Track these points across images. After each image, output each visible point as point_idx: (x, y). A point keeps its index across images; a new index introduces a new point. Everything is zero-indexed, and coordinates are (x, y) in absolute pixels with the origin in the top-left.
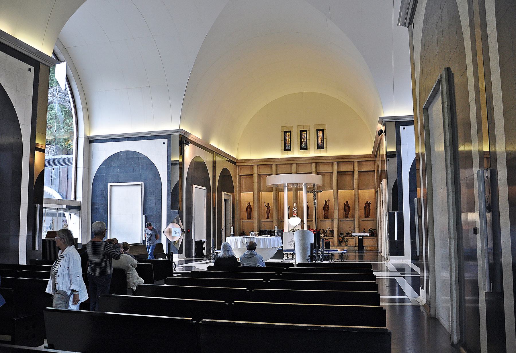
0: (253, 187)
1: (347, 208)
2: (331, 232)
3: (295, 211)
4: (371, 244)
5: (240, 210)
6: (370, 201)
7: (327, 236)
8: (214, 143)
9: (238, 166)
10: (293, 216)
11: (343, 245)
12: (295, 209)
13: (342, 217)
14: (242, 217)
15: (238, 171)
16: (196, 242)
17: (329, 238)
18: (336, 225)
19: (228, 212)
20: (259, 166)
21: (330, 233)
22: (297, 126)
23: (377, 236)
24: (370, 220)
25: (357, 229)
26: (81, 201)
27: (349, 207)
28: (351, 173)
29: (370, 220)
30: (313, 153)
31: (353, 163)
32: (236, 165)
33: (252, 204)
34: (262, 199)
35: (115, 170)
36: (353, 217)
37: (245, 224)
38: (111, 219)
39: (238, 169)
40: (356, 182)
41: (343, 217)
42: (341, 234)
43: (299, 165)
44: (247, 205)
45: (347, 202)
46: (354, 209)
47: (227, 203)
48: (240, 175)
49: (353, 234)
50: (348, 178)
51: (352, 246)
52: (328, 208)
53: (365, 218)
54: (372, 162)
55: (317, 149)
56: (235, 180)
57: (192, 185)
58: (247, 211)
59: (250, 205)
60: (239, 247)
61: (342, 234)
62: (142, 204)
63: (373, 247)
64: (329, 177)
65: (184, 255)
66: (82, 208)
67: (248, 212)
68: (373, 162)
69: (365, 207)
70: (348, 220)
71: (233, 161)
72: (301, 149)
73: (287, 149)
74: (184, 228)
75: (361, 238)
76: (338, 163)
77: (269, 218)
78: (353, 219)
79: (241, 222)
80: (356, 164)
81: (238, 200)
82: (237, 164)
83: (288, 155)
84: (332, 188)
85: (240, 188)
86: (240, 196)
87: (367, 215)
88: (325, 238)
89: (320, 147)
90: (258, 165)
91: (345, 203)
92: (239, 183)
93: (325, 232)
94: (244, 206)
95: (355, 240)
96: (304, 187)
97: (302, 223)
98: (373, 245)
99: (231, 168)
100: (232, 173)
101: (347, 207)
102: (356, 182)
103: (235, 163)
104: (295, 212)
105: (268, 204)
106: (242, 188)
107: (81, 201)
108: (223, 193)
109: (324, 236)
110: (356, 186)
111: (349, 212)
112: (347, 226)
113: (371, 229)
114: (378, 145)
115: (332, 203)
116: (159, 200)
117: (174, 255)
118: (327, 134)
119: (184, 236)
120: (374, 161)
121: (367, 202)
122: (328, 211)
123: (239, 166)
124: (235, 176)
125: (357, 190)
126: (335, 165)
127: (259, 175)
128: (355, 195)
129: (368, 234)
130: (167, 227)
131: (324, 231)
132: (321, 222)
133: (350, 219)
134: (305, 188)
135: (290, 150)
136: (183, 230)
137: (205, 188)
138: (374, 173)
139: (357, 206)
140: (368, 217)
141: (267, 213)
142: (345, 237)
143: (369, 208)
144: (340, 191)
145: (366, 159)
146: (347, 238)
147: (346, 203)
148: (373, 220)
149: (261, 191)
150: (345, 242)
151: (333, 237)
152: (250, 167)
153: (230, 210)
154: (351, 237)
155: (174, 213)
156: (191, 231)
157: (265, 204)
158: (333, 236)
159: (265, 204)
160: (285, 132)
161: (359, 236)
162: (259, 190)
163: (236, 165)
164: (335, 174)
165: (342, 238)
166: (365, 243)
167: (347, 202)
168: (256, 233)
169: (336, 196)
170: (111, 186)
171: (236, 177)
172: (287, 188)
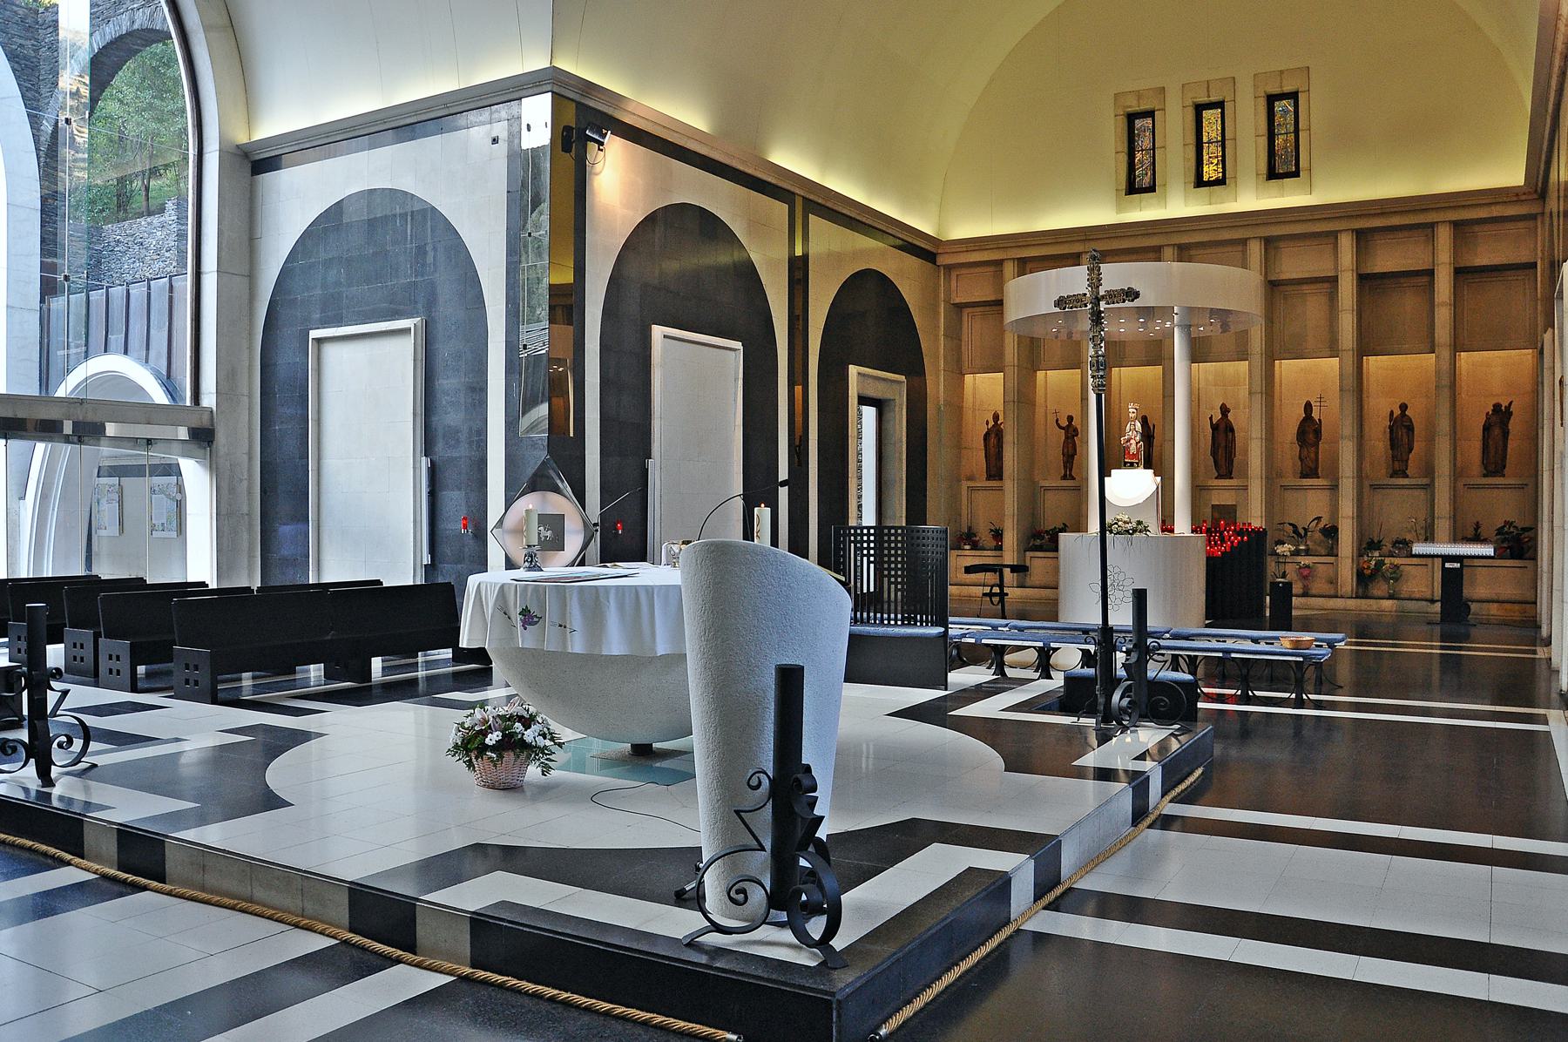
0: (1000, 354)
1: (1401, 433)
2: (1324, 535)
3: (1132, 441)
4: (1509, 591)
5: (959, 445)
6: (1511, 403)
7: (1307, 553)
8: (790, 158)
9: (944, 266)
10: (1125, 463)
11: (1376, 592)
12: (1132, 435)
13: (1380, 474)
17: (1316, 559)
18: (1347, 507)
19: (889, 450)
21: (1322, 538)
22: (1183, 86)
23: (1534, 558)
24: (1507, 487)
25: (1443, 526)
26: (215, 409)
27: (1410, 429)
28: (1425, 279)
29: (1507, 487)
30: (1251, 198)
31: (1430, 235)
35: (332, 275)
36: (1429, 471)
37: (980, 497)
38: (321, 478)
40: (1443, 316)
41: (1384, 471)
42: (1367, 544)
45: (1404, 407)
46: (1431, 439)
47: (887, 416)
48: (960, 307)
49: (1418, 549)
50: (1406, 304)
51: (1418, 596)
52: (1318, 433)
53: (1485, 476)
54: (1521, 224)
58: (985, 446)
61: (1374, 545)
62: (418, 411)
63: (1517, 607)
64: (1323, 299)
66: (221, 437)
67: (993, 451)
68: (1531, 224)
69: (1487, 428)
70: (1403, 487)
71: (922, 249)
73: (1136, 186)
75: (1457, 565)
76: (1362, 236)
77: (1070, 475)
78: (1425, 481)
80: (1444, 236)
82: (941, 260)
83: (1145, 211)
84: (1333, 351)
87: (1494, 463)
88: (1299, 559)
89: (1278, 170)
91: (1392, 413)
93: (1299, 534)
94: (977, 429)
95: (1430, 574)
97: (1165, 494)
98: (1518, 598)
99: (905, 275)
100: (910, 292)
101: (1401, 427)
102: (1443, 316)
107: (215, 409)
109: (1296, 553)
110: (1443, 333)
111: (1411, 450)
112: (1397, 511)
113: (1510, 524)
114: (1550, 110)
115: (1335, 415)
116: (478, 391)
118: (1317, 112)
120: (1533, 217)
121: (1497, 407)
122: (1316, 445)
123: (949, 268)
125: (1446, 353)
126: (1346, 243)
128: (1438, 372)
129: (1488, 550)
131: (1296, 531)
132: (1288, 494)
133: (1413, 481)
134: (1180, 336)
138: (1532, 278)
139: (1444, 425)
141: (1063, 454)
142: (1387, 561)
143: (1505, 434)
144: (1373, 363)
145: (1496, 211)
146: (1397, 561)
147: (1397, 412)
148: (1522, 487)
150: (1386, 580)
151: (1331, 559)
154: (1408, 561)
157: (1057, 421)
158: (1332, 552)
159: (1057, 421)
161: (1447, 558)
165: (1373, 563)
166: (1478, 588)
167: (1404, 407)
168: (677, 551)
169: (1350, 382)
170: (319, 341)
171: (939, 313)
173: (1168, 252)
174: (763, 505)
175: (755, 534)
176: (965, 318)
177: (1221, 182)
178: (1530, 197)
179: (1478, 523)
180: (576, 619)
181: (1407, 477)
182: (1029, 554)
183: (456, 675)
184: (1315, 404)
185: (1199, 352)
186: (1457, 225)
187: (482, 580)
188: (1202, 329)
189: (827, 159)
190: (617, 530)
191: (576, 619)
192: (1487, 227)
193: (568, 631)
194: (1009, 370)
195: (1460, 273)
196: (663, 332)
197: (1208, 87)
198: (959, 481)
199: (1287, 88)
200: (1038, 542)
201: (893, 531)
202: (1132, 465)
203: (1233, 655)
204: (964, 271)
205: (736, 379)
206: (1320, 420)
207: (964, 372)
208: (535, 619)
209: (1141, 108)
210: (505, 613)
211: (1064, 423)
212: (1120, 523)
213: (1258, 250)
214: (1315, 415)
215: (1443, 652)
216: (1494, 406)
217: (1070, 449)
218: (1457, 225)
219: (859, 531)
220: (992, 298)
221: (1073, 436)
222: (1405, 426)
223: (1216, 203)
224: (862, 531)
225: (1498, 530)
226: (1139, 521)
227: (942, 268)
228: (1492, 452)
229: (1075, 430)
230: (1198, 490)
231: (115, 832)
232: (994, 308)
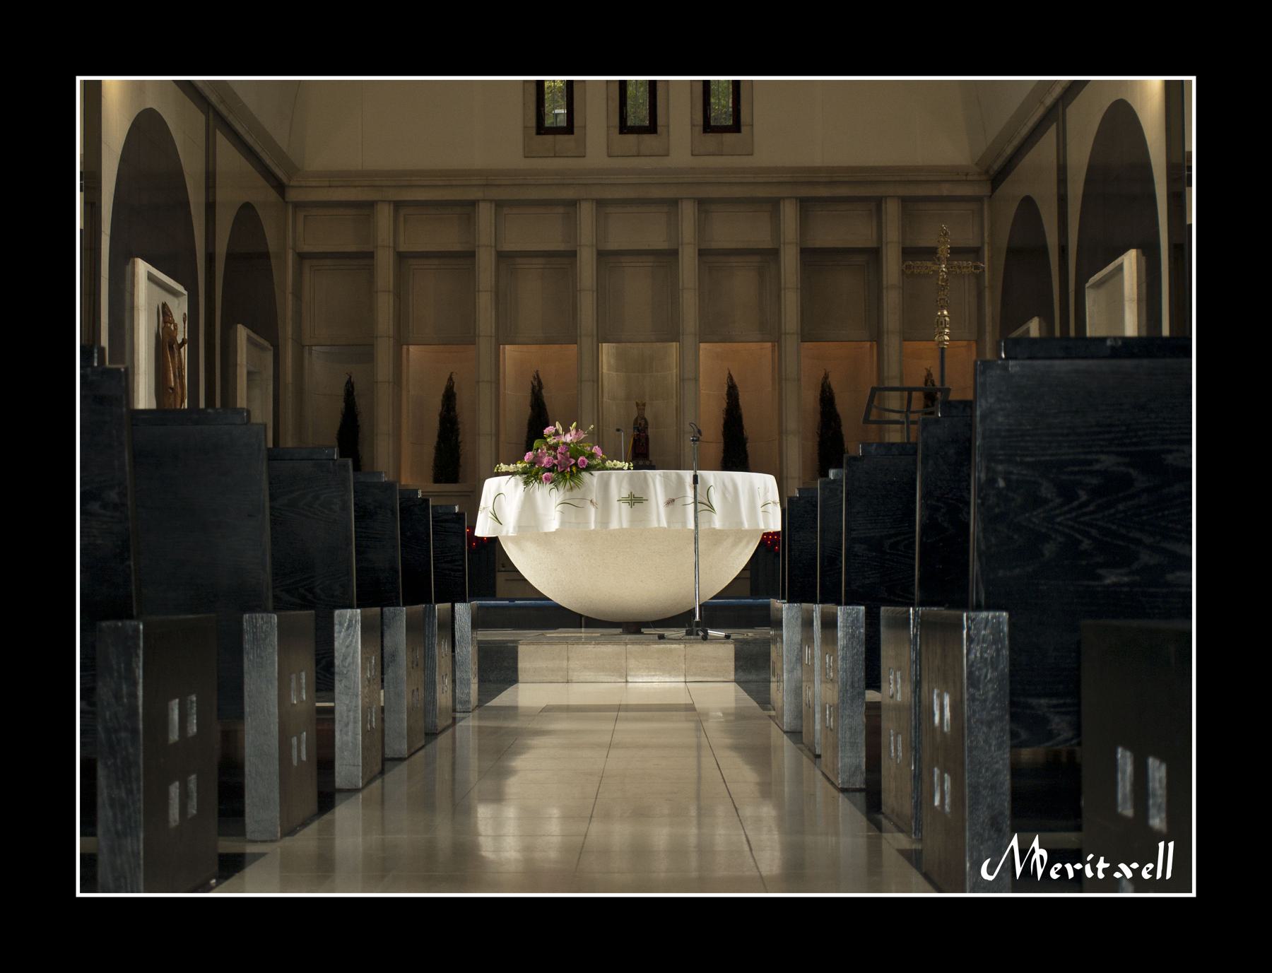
40: (892, 300)
48: (302, 257)
56: (285, 274)
82: (293, 195)
108: (242, 333)
123: (298, 206)
127: (402, 258)
137: (180, 288)
145: (946, 190)
160: (569, 129)
164: (790, 260)
218: (905, 201)
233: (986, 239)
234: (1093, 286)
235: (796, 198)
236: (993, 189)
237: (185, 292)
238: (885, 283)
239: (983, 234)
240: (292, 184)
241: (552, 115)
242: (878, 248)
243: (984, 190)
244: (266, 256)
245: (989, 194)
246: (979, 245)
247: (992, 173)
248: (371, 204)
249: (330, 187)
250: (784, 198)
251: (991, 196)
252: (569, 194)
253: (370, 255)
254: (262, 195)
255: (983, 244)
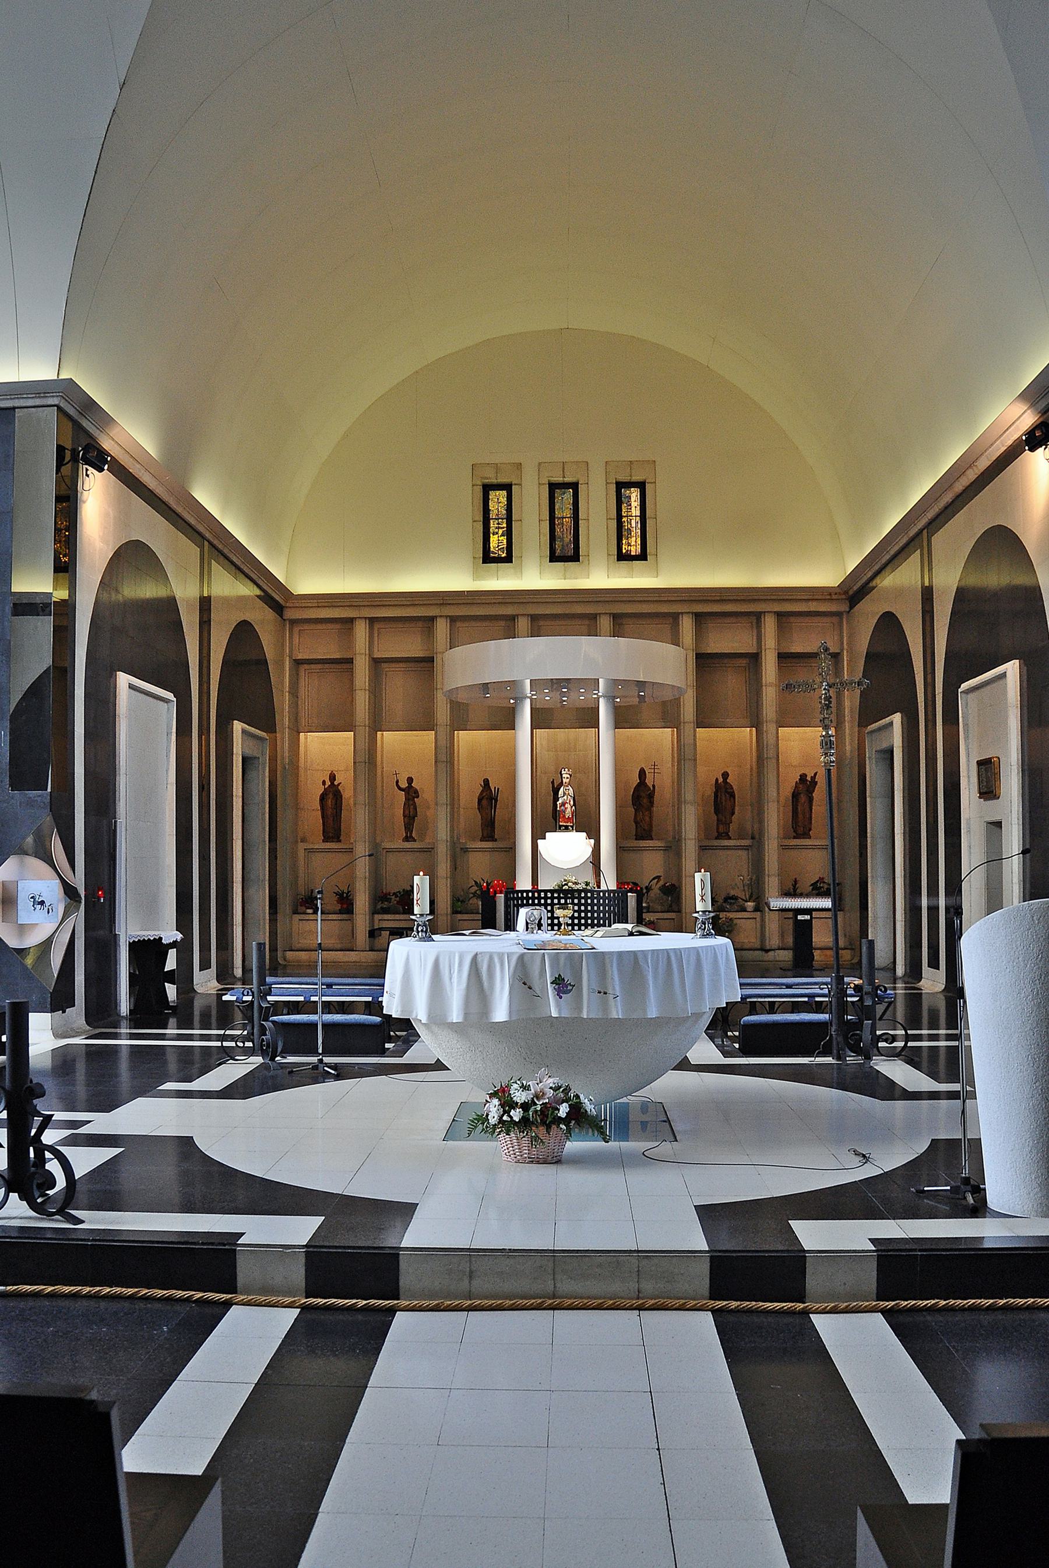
0: (351, 713)
5: (297, 807)
6: (816, 774)
8: (206, 496)
10: (560, 826)
14: (300, 835)
15: (291, 642)
16: (137, 947)
18: (362, 868)
20: (376, 626)
29: (814, 847)
32: (281, 616)
33: (345, 780)
34: (382, 761)
37: (317, 859)
39: (291, 637)
40: (770, 695)
43: (541, 623)
44: (324, 783)
45: (725, 775)
47: (252, 774)
48: (298, 663)
52: (651, 796)
54: (828, 619)
55: (618, 560)
56: (281, 679)
57: (112, 676)
59: (336, 783)
60: (500, 1013)
65: (77, 1014)
68: (835, 619)
69: (795, 795)
70: (728, 848)
72: (554, 558)
74: (79, 882)
75: (808, 917)
76: (699, 618)
77: (411, 836)
79: (301, 854)
80: (770, 625)
81: (291, 762)
82: (289, 614)
85: (297, 713)
86: (295, 744)
90: (372, 621)
91: (717, 780)
92: (294, 692)
94: (313, 789)
96: (601, 700)
103: (278, 608)
104: (569, 810)
105: (410, 780)
106: (302, 714)
108: (238, 726)
111: (733, 813)
117: (32, 1017)
118: (661, 497)
119: (79, 918)
121: (803, 777)
123: (293, 622)
124: (280, 664)
127: (376, 663)
130: (449, 1069)
135: (508, 559)
136: (70, 891)
137: (170, 696)
140: (806, 835)
141: (404, 816)
143: (811, 800)
145: (813, 607)
146: (732, 915)
147: (721, 780)
148: (746, 848)
149: (383, 728)
152: (338, 626)
153: (264, 802)
155: (31, 803)
156: (108, 897)
157: (397, 782)
159: (397, 782)
160: (487, 489)
162: (377, 724)
163: (281, 616)
168: (558, 912)
172: (528, 702)
173: (523, 624)
174: (421, 873)
175: (415, 902)
176: (302, 673)
177: (643, 556)
178: (840, 597)
179: (796, 879)
180: (616, 985)
181: (730, 838)
182: (377, 917)
183: (947, 1035)
184: (650, 771)
185: (623, 719)
186: (779, 615)
187: (479, 950)
188: (618, 700)
189: (226, 503)
190: (99, 898)
191: (616, 985)
192: (800, 619)
193: (611, 996)
194: (441, 730)
195: (784, 657)
196: (128, 680)
197: (564, 468)
198: (297, 842)
199: (636, 478)
200: (385, 905)
201: (583, 895)
202: (566, 828)
203: (817, 999)
204: (306, 627)
205: (169, 734)
206: (654, 786)
207: (301, 729)
208: (570, 988)
209: (499, 481)
210: (525, 984)
211: (404, 784)
212: (570, 884)
213: (608, 626)
214: (649, 781)
215: (910, 991)
216: (800, 776)
217: (411, 810)
218: (779, 615)
219: (536, 895)
220: (420, 654)
221: (414, 798)
222: (728, 793)
223: (570, 579)
224: (539, 895)
225: (812, 885)
226: (586, 882)
227: (288, 622)
228: (800, 816)
229: (416, 792)
230: (621, 850)
231: (304, 1254)
232: (345, 666)
233: (845, 646)
234: (964, 692)
235: (692, 613)
236: (851, 607)
237: (175, 699)
238: (764, 682)
239: (842, 643)
240: (288, 605)
241: (959, 1178)
242: (758, 653)
243: (844, 607)
244: (265, 662)
245: (848, 610)
246: (839, 651)
247: (851, 593)
248: (351, 621)
249: (318, 607)
250: (356, 618)
251: (849, 612)
252: (509, 611)
253: (350, 661)
254: (262, 618)
255: (842, 650)
